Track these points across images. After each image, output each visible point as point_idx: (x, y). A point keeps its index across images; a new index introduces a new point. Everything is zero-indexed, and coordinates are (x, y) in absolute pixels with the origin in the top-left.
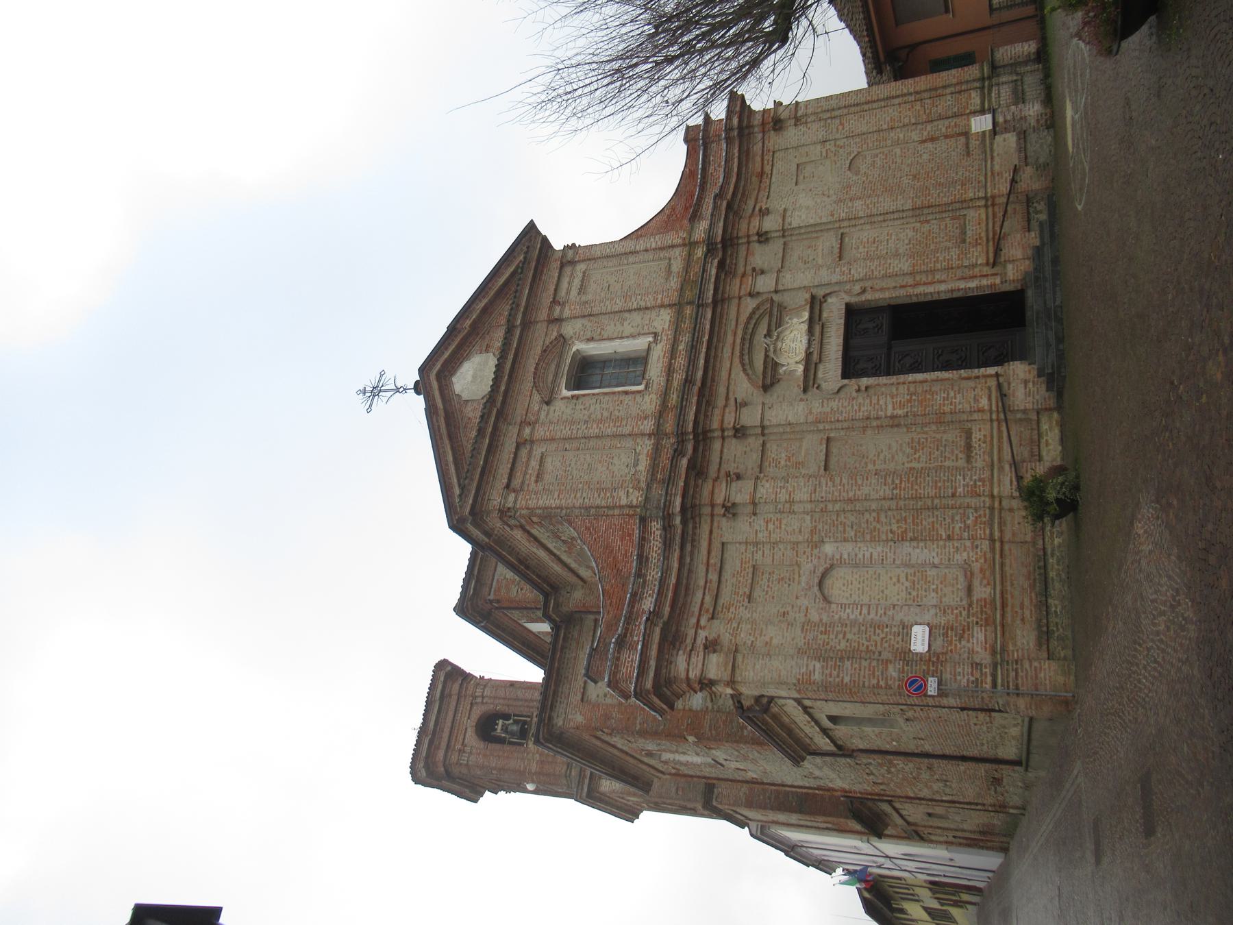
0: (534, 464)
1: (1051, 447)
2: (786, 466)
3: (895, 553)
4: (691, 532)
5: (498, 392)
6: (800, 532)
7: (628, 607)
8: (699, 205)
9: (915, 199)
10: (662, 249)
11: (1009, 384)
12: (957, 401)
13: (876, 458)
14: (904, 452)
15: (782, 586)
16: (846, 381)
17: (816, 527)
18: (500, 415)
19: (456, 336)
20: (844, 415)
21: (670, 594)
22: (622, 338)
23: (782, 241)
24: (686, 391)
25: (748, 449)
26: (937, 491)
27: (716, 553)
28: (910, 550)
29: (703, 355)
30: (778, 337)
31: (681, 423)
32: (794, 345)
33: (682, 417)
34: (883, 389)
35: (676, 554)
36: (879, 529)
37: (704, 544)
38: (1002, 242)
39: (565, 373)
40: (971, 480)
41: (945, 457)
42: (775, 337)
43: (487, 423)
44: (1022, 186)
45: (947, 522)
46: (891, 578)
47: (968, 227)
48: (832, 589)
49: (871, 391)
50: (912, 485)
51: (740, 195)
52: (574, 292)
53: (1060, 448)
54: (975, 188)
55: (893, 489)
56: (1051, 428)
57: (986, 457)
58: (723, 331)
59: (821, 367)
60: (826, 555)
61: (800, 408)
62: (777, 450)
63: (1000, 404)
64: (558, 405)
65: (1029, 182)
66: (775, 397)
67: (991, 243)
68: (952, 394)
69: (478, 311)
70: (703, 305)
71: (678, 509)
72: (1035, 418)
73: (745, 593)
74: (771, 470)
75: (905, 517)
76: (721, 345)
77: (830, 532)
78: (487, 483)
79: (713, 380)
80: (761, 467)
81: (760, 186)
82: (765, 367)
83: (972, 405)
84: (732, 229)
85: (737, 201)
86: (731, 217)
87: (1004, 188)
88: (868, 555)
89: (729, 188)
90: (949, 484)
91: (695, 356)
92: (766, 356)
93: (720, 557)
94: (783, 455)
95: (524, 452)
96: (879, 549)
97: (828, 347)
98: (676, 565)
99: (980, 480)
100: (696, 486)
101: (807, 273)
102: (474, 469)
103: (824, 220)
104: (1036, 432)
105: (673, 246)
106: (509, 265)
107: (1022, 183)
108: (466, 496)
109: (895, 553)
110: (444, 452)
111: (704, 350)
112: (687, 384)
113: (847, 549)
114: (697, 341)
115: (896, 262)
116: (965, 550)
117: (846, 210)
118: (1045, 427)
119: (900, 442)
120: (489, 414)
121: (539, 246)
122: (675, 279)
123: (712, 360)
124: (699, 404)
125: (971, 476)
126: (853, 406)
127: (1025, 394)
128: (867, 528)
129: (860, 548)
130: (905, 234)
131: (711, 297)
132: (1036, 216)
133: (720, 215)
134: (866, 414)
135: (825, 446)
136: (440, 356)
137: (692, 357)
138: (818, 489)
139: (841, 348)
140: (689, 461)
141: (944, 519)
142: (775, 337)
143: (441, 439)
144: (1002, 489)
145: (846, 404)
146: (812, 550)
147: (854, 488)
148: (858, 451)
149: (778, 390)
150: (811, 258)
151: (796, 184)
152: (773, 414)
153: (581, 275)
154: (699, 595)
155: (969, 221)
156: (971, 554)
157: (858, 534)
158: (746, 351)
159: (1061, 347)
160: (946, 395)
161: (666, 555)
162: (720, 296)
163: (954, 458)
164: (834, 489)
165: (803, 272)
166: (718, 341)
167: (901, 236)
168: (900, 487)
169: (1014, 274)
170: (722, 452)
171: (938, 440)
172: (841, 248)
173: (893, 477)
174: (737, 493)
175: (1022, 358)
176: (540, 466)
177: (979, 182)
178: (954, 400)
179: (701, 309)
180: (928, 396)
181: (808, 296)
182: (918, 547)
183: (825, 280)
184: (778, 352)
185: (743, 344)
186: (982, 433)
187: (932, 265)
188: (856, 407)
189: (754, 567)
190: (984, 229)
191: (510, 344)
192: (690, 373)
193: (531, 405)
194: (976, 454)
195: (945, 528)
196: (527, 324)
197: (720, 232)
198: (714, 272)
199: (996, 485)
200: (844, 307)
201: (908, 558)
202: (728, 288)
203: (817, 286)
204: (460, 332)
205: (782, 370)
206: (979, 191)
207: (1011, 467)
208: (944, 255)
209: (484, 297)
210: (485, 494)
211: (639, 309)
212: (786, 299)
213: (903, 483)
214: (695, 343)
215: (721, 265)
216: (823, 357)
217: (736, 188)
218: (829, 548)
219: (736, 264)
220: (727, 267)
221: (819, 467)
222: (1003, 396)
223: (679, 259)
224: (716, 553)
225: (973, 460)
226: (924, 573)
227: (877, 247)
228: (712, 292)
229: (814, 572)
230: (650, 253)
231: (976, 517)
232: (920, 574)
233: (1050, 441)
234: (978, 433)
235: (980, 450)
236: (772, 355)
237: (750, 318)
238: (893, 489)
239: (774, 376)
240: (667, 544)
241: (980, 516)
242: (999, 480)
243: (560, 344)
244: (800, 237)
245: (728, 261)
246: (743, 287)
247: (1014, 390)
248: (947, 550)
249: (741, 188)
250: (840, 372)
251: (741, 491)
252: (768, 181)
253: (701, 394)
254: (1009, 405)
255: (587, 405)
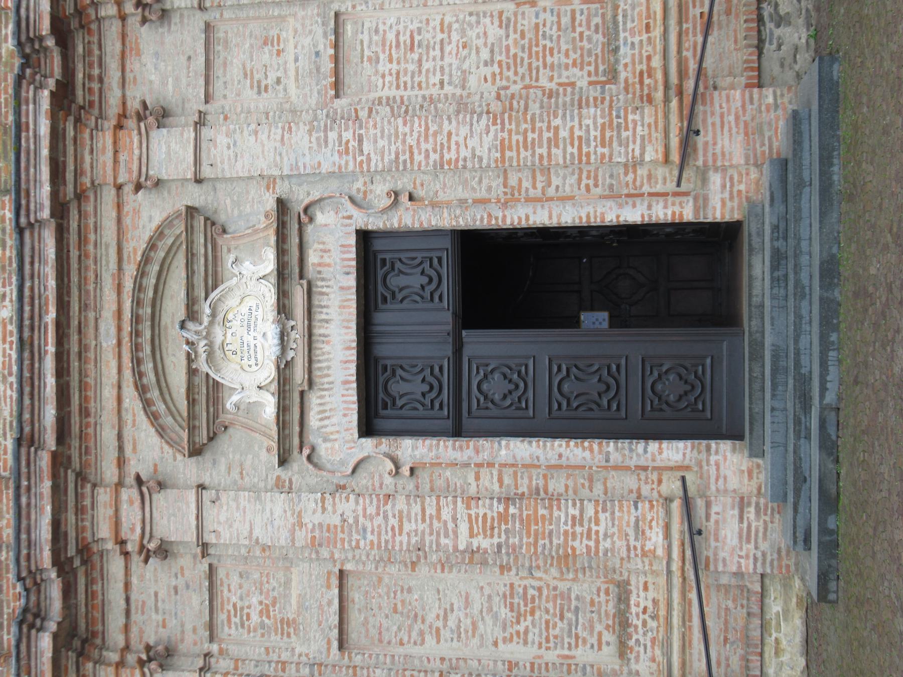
1: (785, 658)
11: (708, 505)
12: (602, 529)
13: (440, 624)
14: (496, 617)
16: (369, 443)
20: (369, 537)
23: (199, 20)
24: (24, 470)
29: (49, 364)
31: (24, 552)
33: (24, 536)
34: (448, 473)
41: (577, 637)
42: (206, 320)
47: (622, 35)
53: (802, 662)
57: (658, 652)
58: (91, 275)
59: (313, 400)
61: (278, 511)
62: (241, 587)
66: (223, 468)
68: (590, 511)
70: (30, 225)
74: (233, 631)
76: (91, 315)
79: (85, 412)
80: (211, 627)
82: (192, 402)
83: (632, 543)
91: (32, 370)
92: (192, 372)
94: (255, 600)
97: (327, 348)
101: (263, 136)
104: (757, 622)
111: (51, 349)
112: (23, 451)
114: (32, 329)
115: (464, 131)
118: (775, 607)
119: (487, 591)
123: (75, 364)
124: (57, 490)
126: (386, 517)
130: (480, 29)
131: (47, 203)
132: (778, 32)
134: (414, 540)
135: (336, 591)
137: (27, 374)
145: (371, 510)
148: (403, 602)
150: (272, 77)
152: (222, 518)
159: (831, 523)
162: (70, 188)
163: (594, 640)
165: (256, 133)
166: (84, 307)
167: (472, 34)
170: (127, 586)
171: (562, 595)
172: (336, 59)
179: (27, 234)
180: (542, 511)
184: (218, 353)
186: (651, 594)
187: (544, 151)
188: (392, 521)
190: (659, 47)
194: (637, 641)
198: (44, 128)
200: (352, 240)
202: (87, 158)
203: (289, 177)
216: (316, 373)
219: (101, 80)
220: (79, 93)
221: (329, 642)
222: (694, 533)
225: (632, 656)
227: (420, 61)
228: (46, 189)
233: (784, 643)
234: (642, 594)
235: (645, 634)
236: (204, 367)
237: (146, 260)
239: (216, 416)
244: (243, 14)
245: (80, 76)
246: (122, 158)
247: (717, 522)
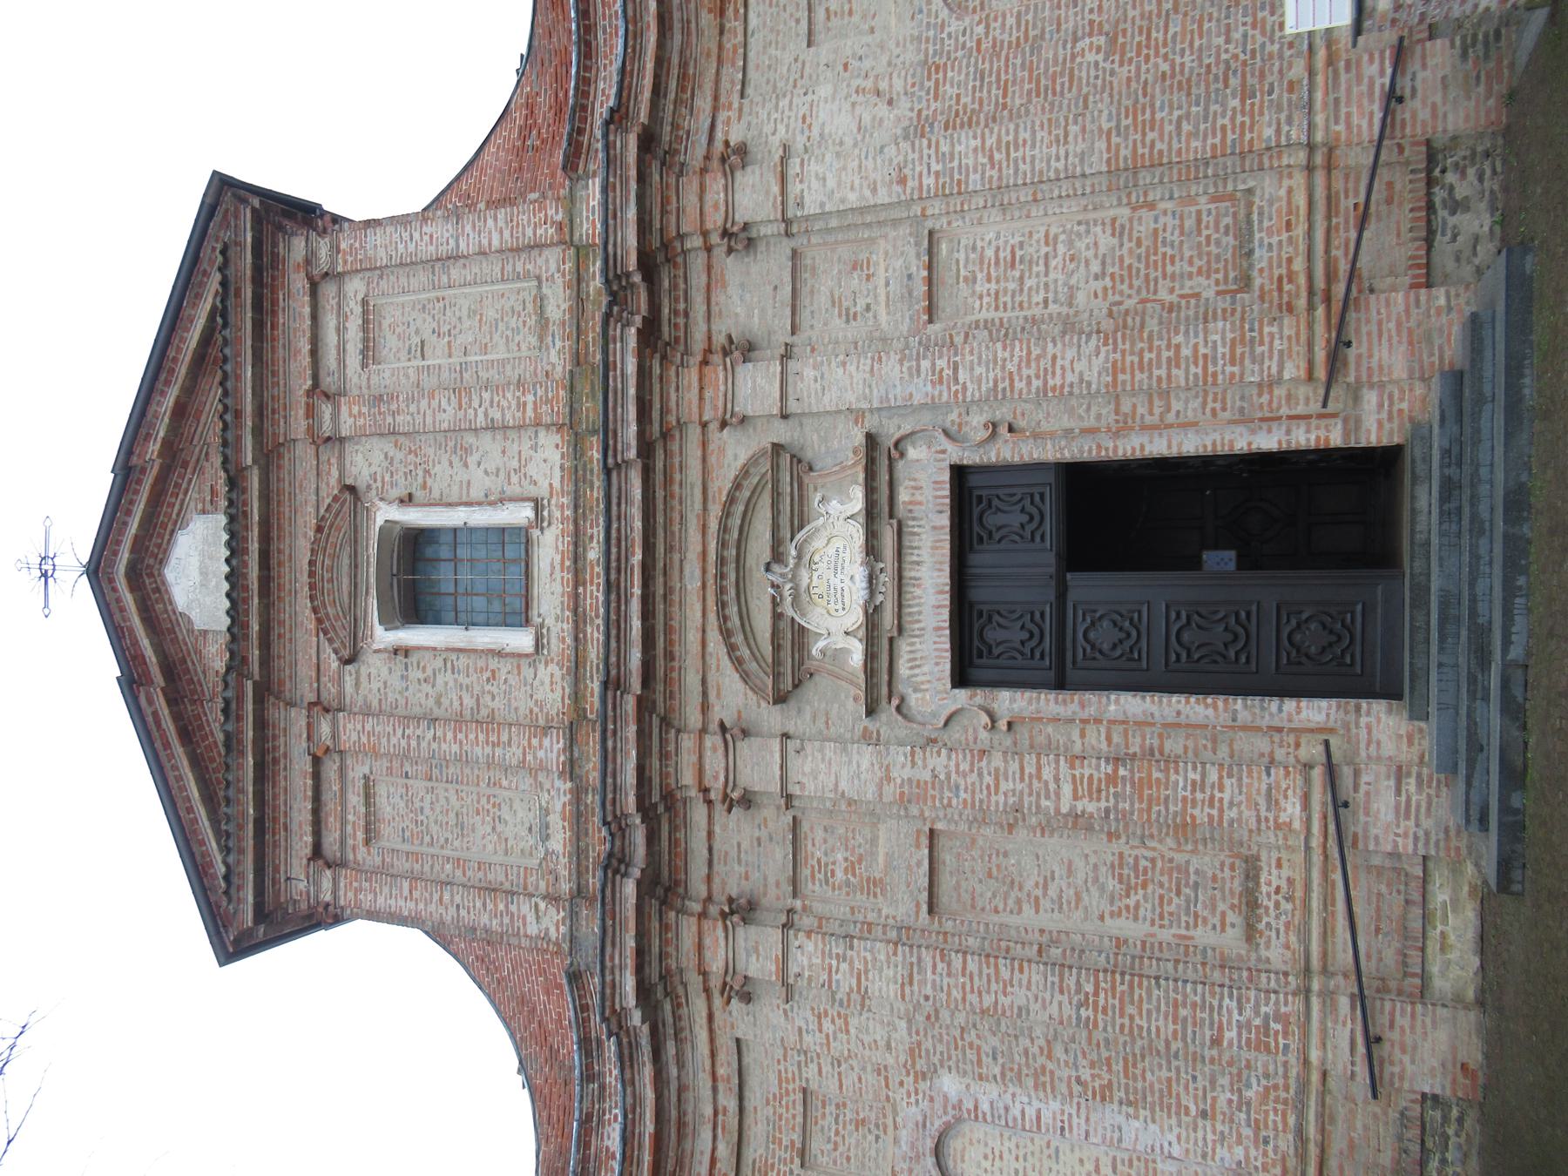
0: (355, 800)
1: (1453, 956)
2: (848, 883)
3: (1087, 1120)
4: (670, 1020)
5: (246, 637)
6: (888, 1047)
7: (578, 1151)
8: (584, 108)
9: (1115, 140)
10: (517, 250)
11: (1357, 774)
12: (1226, 796)
13: (1039, 892)
14: (1102, 889)
15: (864, 1137)
17: (919, 1044)
18: (266, 690)
19: (139, 482)
20: (962, 795)
21: (647, 1158)
22: (468, 504)
23: (786, 246)
24: (610, 713)
25: (764, 834)
26: (1179, 1027)
27: (726, 1056)
28: (1121, 1119)
29: (635, 606)
30: (799, 557)
31: (610, 796)
32: (837, 581)
33: (610, 780)
35: (648, 1071)
36: (1052, 1072)
37: (702, 1035)
38: (1352, 316)
39: (373, 580)
40: (1257, 1013)
41: (1196, 916)
42: (792, 562)
43: (239, 718)
44: (1418, 115)
45: (1200, 1084)
46: (1081, 1161)
47: (1257, 236)
48: (963, 1161)
49: (1023, 733)
50: (1122, 1001)
51: (673, 85)
52: (353, 360)
54: (1279, 109)
55: (1080, 1005)
56: (1455, 901)
57: (1293, 939)
59: (903, 647)
60: (946, 1097)
61: (865, 764)
62: (825, 841)
63: (1332, 828)
64: (374, 667)
65: (1438, 99)
66: (808, 716)
67: (1320, 312)
68: (1213, 776)
69: (166, 420)
70: (618, 466)
71: (631, 1001)
72: (1419, 872)
73: (792, 1142)
75: (1108, 1059)
76: (676, 557)
77: (950, 1058)
78: (276, 845)
79: (669, 656)
80: (794, 882)
81: (720, 47)
82: (777, 648)
83: (1263, 813)
84: (664, 212)
85: (668, 118)
86: (656, 177)
87: (1365, 118)
88: (1031, 1112)
89: (641, 69)
90: (1206, 1015)
92: (777, 616)
93: (735, 1066)
94: (840, 856)
95: (330, 769)
96: (1055, 1105)
97: (918, 592)
98: (650, 1095)
99: (1278, 1017)
100: (665, 927)
102: (241, 827)
103: (883, 197)
105: (538, 246)
106: (198, 296)
107: (1417, 104)
108: (239, 888)
109: (1087, 1120)
110: (179, 778)
112: (610, 694)
113: (987, 1095)
115: (1071, 353)
116: (1239, 1142)
117: (935, 167)
119: (1092, 860)
120: (240, 699)
121: (249, 240)
122: (559, 344)
123: (660, 607)
124: (643, 736)
125: (1257, 1005)
126: (980, 775)
127: (1397, 808)
128: (1027, 1065)
129: (1014, 1095)
130: (1090, 240)
131: (634, 443)
132: (1452, 221)
133: (625, 182)
134: (1011, 800)
135: (926, 851)
136: (121, 532)
137: (613, 617)
138: (916, 977)
139: (946, 600)
140: (639, 883)
141: (1194, 1078)
142: (792, 562)
143: (167, 745)
144: (1330, 1056)
145: (964, 766)
146: (916, 1081)
147: (994, 986)
148: (998, 866)
149: (815, 695)
151: (809, 45)
152: (807, 769)
153: (358, 310)
154: (706, 1134)
155: (1261, 214)
156: (1253, 1152)
157: (1009, 1074)
158: (732, 592)
159: (1516, 800)
160: (1198, 777)
161: (628, 1075)
163: (1216, 921)
164: (952, 981)
165: (844, 364)
166: (669, 549)
167: (1080, 245)
168: (1096, 1003)
169: (1380, 424)
170: (710, 834)
171: (1179, 869)
172: (930, 281)
173: (1079, 975)
174: (748, 955)
175: (1391, 693)
176: (367, 804)
177: (1291, 88)
178: (1218, 795)
181: (859, 439)
182: (1136, 1117)
183: (898, 393)
184: (805, 597)
185: (723, 576)
186: (1285, 873)
187: (1163, 372)
188: (988, 779)
189: (804, 1091)
190: (1302, 247)
191: (245, 513)
192: (613, 659)
193: (322, 656)
195: (1195, 1097)
196: (271, 454)
197: (632, 241)
199: (1315, 1040)
200: (946, 476)
201: (1116, 1135)
204: (143, 471)
205: (816, 649)
206: (1289, 121)
207: (1353, 1008)
208: (1193, 341)
209: (167, 383)
210: (276, 869)
211: (492, 427)
212: (812, 441)
213: (1102, 995)
214: (613, 576)
215: (650, 335)
216: (906, 619)
217: (661, 61)
218: (950, 1084)
219: (686, 315)
221: (918, 905)
223: (559, 281)
224: (726, 1056)
225: (1262, 941)
226: (1151, 1165)
227: (1021, 278)
229: (924, 1126)
230: (492, 257)
231: (1267, 1089)
232: (1142, 1165)
233: (1452, 938)
234: (1274, 872)
237: (731, 500)
238: (1080, 1005)
239: (801, 663)
240: (627, 1060)
241: (1276, 1087)
242: (1324, 1031)
243: (346, 508)
244: (831, 239)
247: (1367, 794)
248: (1200, 1134)
249: (675, 60)
250: (947, 667)
251: (756, 951)
252: (739, 25)
253: (645, 706)
254: (1355, 835)
255: (429, 672)
